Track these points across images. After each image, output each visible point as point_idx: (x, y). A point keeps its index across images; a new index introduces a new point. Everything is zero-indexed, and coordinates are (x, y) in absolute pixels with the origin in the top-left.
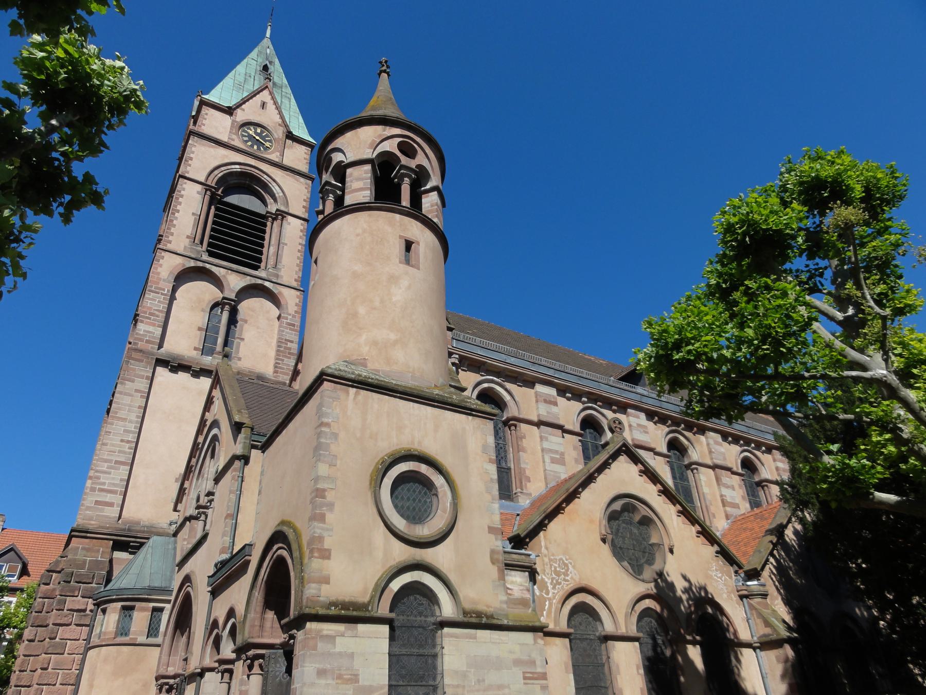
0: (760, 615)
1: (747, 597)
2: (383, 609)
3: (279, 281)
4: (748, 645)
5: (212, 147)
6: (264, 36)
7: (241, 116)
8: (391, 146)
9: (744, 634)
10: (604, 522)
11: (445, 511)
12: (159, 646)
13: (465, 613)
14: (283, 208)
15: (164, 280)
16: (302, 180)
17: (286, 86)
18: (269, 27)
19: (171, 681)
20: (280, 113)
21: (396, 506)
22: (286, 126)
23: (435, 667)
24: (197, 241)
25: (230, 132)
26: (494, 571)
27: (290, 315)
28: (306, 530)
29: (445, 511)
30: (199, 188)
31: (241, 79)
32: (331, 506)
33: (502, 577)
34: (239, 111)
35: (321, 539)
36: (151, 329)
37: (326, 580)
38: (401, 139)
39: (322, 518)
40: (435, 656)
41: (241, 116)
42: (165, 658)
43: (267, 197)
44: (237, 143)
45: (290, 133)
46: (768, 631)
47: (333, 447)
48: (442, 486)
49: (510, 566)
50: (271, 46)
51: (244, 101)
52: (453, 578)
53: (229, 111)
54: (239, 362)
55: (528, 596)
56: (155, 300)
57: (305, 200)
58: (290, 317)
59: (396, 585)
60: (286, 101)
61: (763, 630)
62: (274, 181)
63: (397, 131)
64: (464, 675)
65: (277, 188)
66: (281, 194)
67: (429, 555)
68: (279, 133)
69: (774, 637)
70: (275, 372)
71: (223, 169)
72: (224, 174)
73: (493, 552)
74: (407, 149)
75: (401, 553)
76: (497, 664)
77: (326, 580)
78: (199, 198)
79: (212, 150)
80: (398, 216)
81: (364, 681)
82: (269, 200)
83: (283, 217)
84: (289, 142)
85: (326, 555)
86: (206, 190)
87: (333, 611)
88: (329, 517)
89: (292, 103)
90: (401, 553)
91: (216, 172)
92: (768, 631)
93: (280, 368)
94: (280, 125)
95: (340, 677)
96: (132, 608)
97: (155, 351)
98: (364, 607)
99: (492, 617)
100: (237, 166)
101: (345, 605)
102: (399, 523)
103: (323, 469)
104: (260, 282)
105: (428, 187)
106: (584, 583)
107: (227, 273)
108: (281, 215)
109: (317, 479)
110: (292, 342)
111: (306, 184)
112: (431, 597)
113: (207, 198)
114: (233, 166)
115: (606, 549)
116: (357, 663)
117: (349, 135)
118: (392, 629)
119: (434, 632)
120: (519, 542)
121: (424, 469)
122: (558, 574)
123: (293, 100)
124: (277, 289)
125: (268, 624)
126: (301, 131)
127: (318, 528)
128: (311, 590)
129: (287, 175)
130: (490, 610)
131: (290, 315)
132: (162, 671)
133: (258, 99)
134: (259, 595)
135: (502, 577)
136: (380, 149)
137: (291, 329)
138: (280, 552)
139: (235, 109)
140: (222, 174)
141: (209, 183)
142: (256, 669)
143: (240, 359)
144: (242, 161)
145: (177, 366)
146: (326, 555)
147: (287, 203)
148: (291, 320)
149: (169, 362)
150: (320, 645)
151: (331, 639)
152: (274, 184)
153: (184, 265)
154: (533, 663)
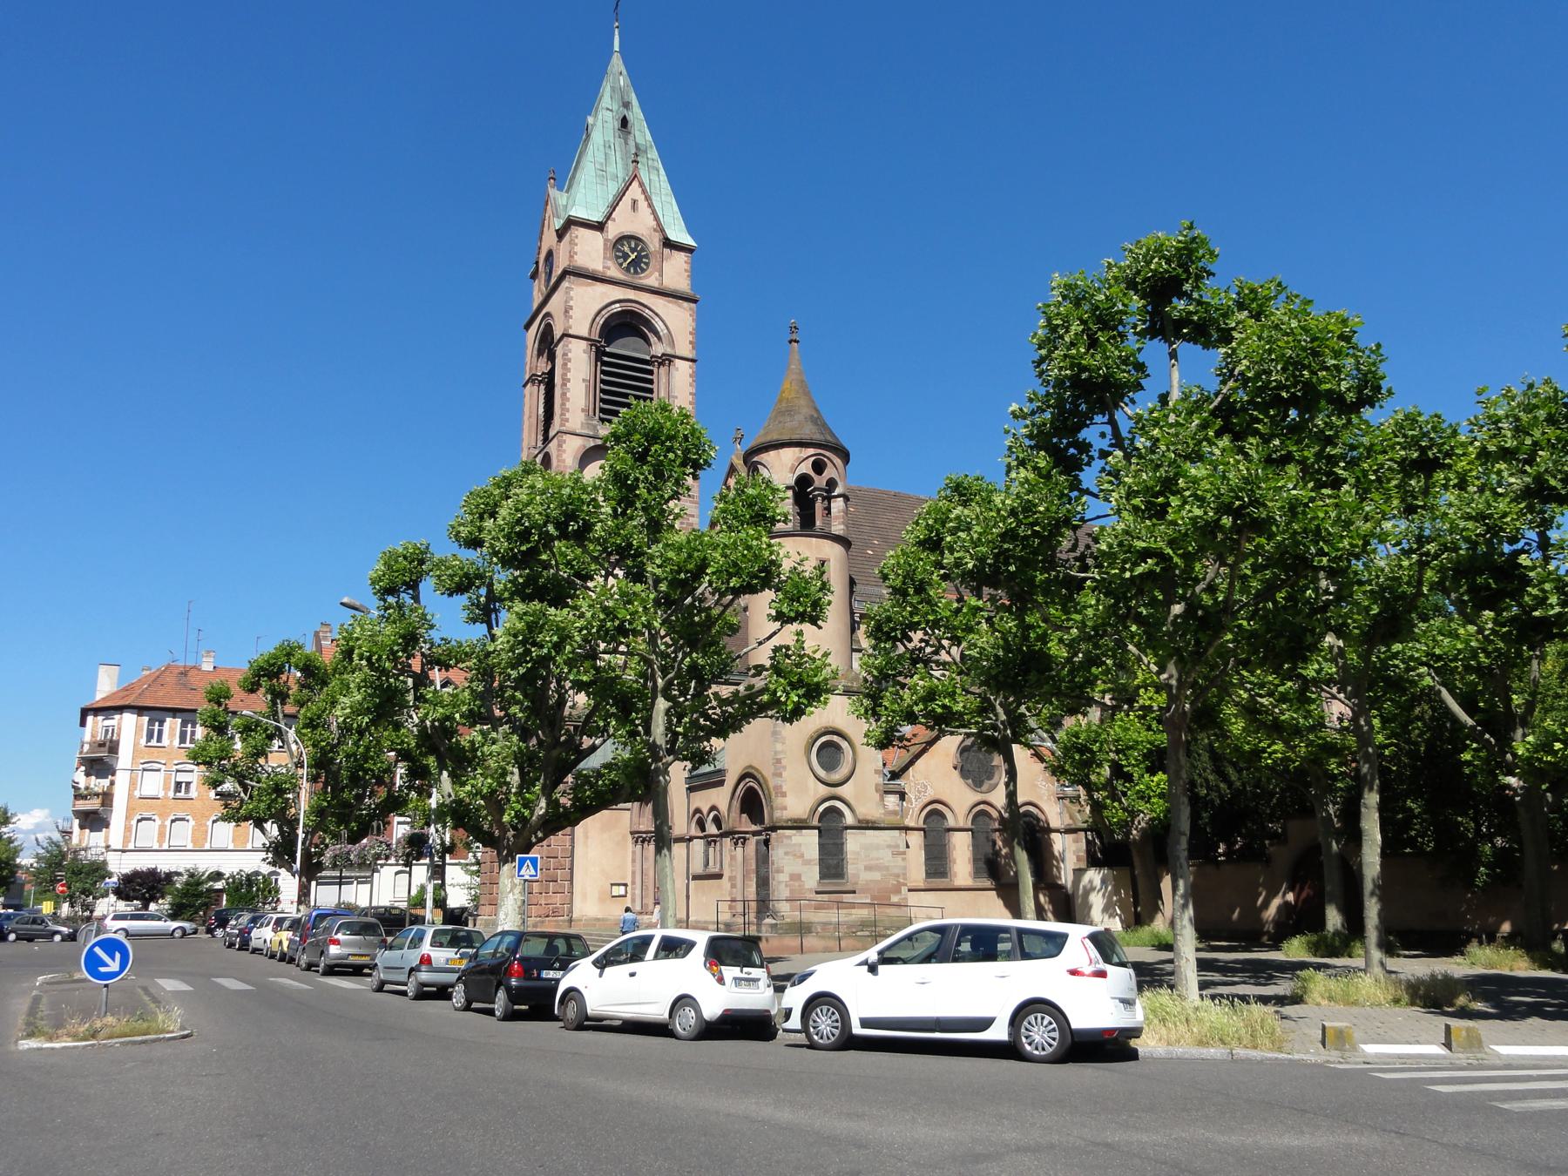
0: (1068, 812)
1: (1062, 798)
2: (815, 822)
4: (1057, 831)
5: (589, 285)
6: (612, 52)
7: (613, 230)
8: (806, 468)
9: (1055, 822)
10: (958, 755)
12: (628, 810)
13: (859, 821)
14: (669, 351)
16: (686, 304)
17: (651, 146)
18: (617, 31)
19: (644, 835)
20: (654, 212)
21: (819, 762)
22: (662, 230)
23: (842, 849)
24: (591, 413)
25: (604, 258)
26: (877, 796)
28: (767, 771)
30: (584, 344)
31: (601, 158)
32: (785, 768)
33: (882, 799)
35: (781, 786)
37: (785, 808)
38: (813, 458)
39: (780, 775)
40: (843, 844)
41: (613, 230)
42: (635, 819)
43: (650, 335)
44: (614, 272)
46: (1071, 822)
47: (783, 732)
49: (887, 792)
50: (625, 72)
51: (614, 207)
52: (852, 802)
53: (600, 227)
55: (897, 808)
57: (691, 333)
59: (821, 809)
60: (654, 177)
61: (1068, 821)
62: (657, 314)
63: (811, 451)
64: (858, 853)
65: (660, 323)
66: (666, 331)
67: (839, 791)
68: (654, 244)
69: (1073, 826)
71: (603, 312)
72: (606, 319)
73: (877, 785)
74: (819, 467)
75: (824, 791)
76: (878, 847)
77: (785, 808)
78: (585, 357)
79: (589, 289)
81: (807, 856)
82: (653, 339)
83: (670, 361)
84: (667, 251)
85: (784, 795)
86: (591, 345)
87: (790, 824)
88: (784, 774)
90: (824, 791)
91: (598, 319)
92: (1071, 822)
94: (655, 230)
98: (804, 821)
99: (875, 822)
100: (618, 305)
101: (795, 821)
102: (822, 773)
103: (779, 747)
105: (835, 494)
106: (938, 797)
108: (667, 360)
109: (776, 753)
110: (693, 516)
111: (690, 309)
112: (840, 814)
113: (593, 354)
114: (613, 306)
115: (956, 773)
116: (803, 849)
117: (772, 453)
118: (820, 832)
119: (842, 831)
120: (895, 775)
121: (835, 738)
122: (919, 792)
123: (662, 172)
125: (743, 820)
126: (679, 234)
127: (778, 781)
128: (777, 814)
129: (669, 302)
130: (873, 819)
132: (635, 828)
133: (627, 199)
134: (736, 804)
135: (882, 799)
136: (798, 473)
137: (691, 502)
138: (751, 784)
139: (606, 222)
140: (603, 320)
142: (740, 844)
144: (622, 297)
146: (784, 795)
147: (672, 343)
150: (785, 840)
152: (657, 319)
153: (584, 446)
154: (898, 846)
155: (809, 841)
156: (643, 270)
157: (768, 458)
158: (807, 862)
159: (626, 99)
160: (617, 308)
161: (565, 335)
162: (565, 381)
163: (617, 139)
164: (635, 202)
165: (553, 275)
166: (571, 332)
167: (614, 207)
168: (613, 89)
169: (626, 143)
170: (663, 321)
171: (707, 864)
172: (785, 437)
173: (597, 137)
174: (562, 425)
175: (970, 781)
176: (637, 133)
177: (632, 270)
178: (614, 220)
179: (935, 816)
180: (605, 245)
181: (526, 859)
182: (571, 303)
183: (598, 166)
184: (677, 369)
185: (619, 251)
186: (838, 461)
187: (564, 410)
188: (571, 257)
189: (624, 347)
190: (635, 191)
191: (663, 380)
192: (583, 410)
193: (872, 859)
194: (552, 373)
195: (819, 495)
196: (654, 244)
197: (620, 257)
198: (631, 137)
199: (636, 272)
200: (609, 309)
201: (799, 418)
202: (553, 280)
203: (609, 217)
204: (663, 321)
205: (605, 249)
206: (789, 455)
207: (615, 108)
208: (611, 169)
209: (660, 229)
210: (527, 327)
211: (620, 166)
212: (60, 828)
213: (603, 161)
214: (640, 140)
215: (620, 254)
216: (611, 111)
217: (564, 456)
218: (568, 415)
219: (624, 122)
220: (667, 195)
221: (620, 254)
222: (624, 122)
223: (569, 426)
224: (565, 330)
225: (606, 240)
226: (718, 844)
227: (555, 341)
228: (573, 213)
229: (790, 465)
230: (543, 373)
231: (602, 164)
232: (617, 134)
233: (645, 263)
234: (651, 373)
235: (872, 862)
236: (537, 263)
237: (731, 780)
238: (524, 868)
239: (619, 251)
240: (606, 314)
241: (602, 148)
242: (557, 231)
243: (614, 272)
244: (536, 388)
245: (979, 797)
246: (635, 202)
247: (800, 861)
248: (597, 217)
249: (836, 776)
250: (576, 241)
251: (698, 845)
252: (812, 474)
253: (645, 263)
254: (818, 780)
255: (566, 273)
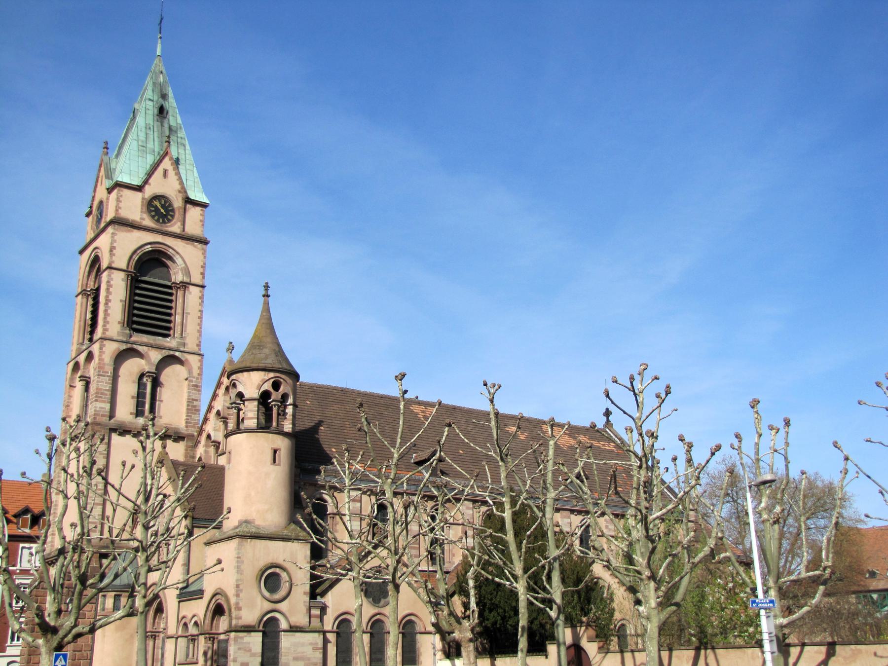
2: (261, 628)
3: (185, 349)
5: (129, 231)
7: (149, 191)
8: (268, 386)
11: (285, 588)
15: (107, 365)
22: (186, 192)
25: (141, 212)
27: (194, 378)
29: (285, 588)
31: (142, 136)
34: (147, 187)
36: (103, 405)
41: (149, 191)
45: (188, 198)
48: (285, 577)
51: (150, 174)
52: (287, 614)
53: (139, 189)
54: (161, 420)
56: (103, 382)
58: (194, 380)
62: (178, 253)
63: (272, 375)
70: (187, 426)
71: (138, 252)
74: (276, 385)
75: (268, 606)
76: (303, 645)
80: (271, 435)
81: (253, 651)
83: (186, 287)
84: (188, 206)
86: (128, 276)
87: (243, 629)
89: (187, 152)
90: (268, 606)
93: (191, 423)
94: (180, 192)
95: (245, 650)
96: (120, 596)
97: (108, 422)
98: (254, 627)
99: (302, 628)
100: (149, 246)
102: (267, 594)
104: (172, 353)
107: (149, 349)
114: (146, 247)
116: (251, 646)
117: (245, 374)
123: (188, 147)
124: (184, 357)
131: (194, 378)
133: (160, 170)
136: (262, 389)
137: (195, 390)
138: (219, 601)
140: (138, 257)
141: (129, 270)
143: (161, 417)
144: (152, 240)
145: (124, 431)
148: (196, 382)
149: (117, 429)
151: (242, 638)
153: (119, 349)
155: (255, 640)
156: (169, 221)
157: (243, 377)
158: (253, 655)
159: (164, 92)
160: (148, 248)
161: (110, 268)
162: (108, 301)
163: (156, 123)
164: (165, 172)
165: (103, 220)
166: (114, 265)
167: (150, 174)
168: (154, 84)
169: (162, 125)
170: (182, 258)
171: (187, 656)
172: (255, 365)
173: (140, 120)
174: (104, 333)
175: (371, 599)
176: (171, 118)
177: (161, 220)
178: (150, 185)
179: (343, 626)
180: (142, 202)
181: (60, 655)
182: (115, 245)
183: (140, 143)
184: (190, 293)
185: (153, 206)
186: (290, 381)
187: (106, 322)
188: (117, 210)
189: (151, 276)
190: (167, 164)
191: (180, 301)
192: (119, 323)
193: (299, 653)
194: (98, 290)
195: (275, 405)
196: (178, 203)
197: (152, 211)
198: (166, 121)
199: (164, 222)
200: (143, 249)
201: (266, 351)
202: (102, 225)
203: (146, 182)
204: (182, 258)
205: (142, 205)
206: (256, 377)
207: (156, 98)
208: (150, 145)
209: (183, 190)
210: (81, 252)
211: (156, 143)
212: (95, 623)
213: (144, 139)
214: (173, 123)
215: (153, 209)
216: (152, 101)
217: (104, 356)
218: (108, 326)
219: (162, 111)
220: (189, 154)
221: (153, 209)
222: (162, 111)
223: (109, 334)
224: (109, 264)
225: (143, 199)
226: (196, 641)
227: (102, 271)
228: (120, 179)
229: (257, 384)
230: (92, 290)
231: (142, 142)
232: (155, 119)
233: (171, 216)
234: (171, 294)
235: (299, 655)
236: (91, 207)
237: (207, 596)
238: (58, 661)
239: (153, 206)
240: (140, 253)
241: (144, 130)
242: (108, 189)
243: (148, 222)
244: (85, 300)
245: (376, 610)
246: (165, 172)
247: (249, 654)
248: (137, 182)
249: (277, 596)
250: (121, 199)
251: (182, 642)
252: (271, 390)
253: (171, 216)
254: (267, 600)
255: (112, 222)
